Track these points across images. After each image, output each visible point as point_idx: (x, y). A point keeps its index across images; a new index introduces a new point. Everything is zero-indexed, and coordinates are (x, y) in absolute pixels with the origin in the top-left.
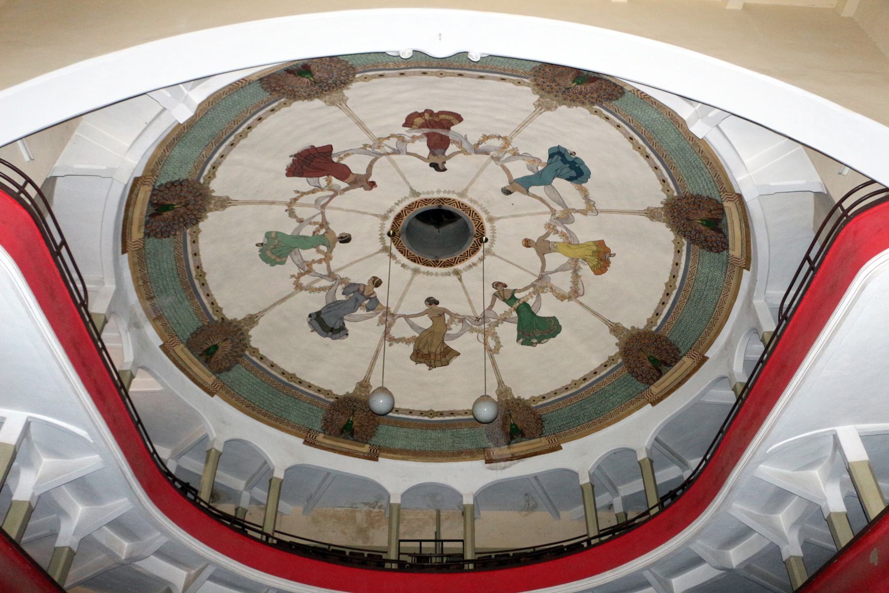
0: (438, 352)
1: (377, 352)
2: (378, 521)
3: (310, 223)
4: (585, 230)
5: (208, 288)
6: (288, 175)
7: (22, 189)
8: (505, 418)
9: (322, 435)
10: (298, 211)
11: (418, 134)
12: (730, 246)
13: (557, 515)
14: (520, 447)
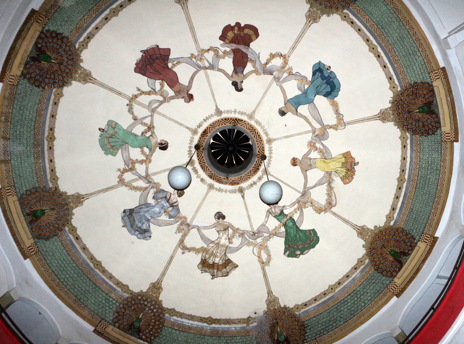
4: (336, 144)
5: (53, 153)
6: (136, 71)
8: (273, 327)
11: (228, 49)
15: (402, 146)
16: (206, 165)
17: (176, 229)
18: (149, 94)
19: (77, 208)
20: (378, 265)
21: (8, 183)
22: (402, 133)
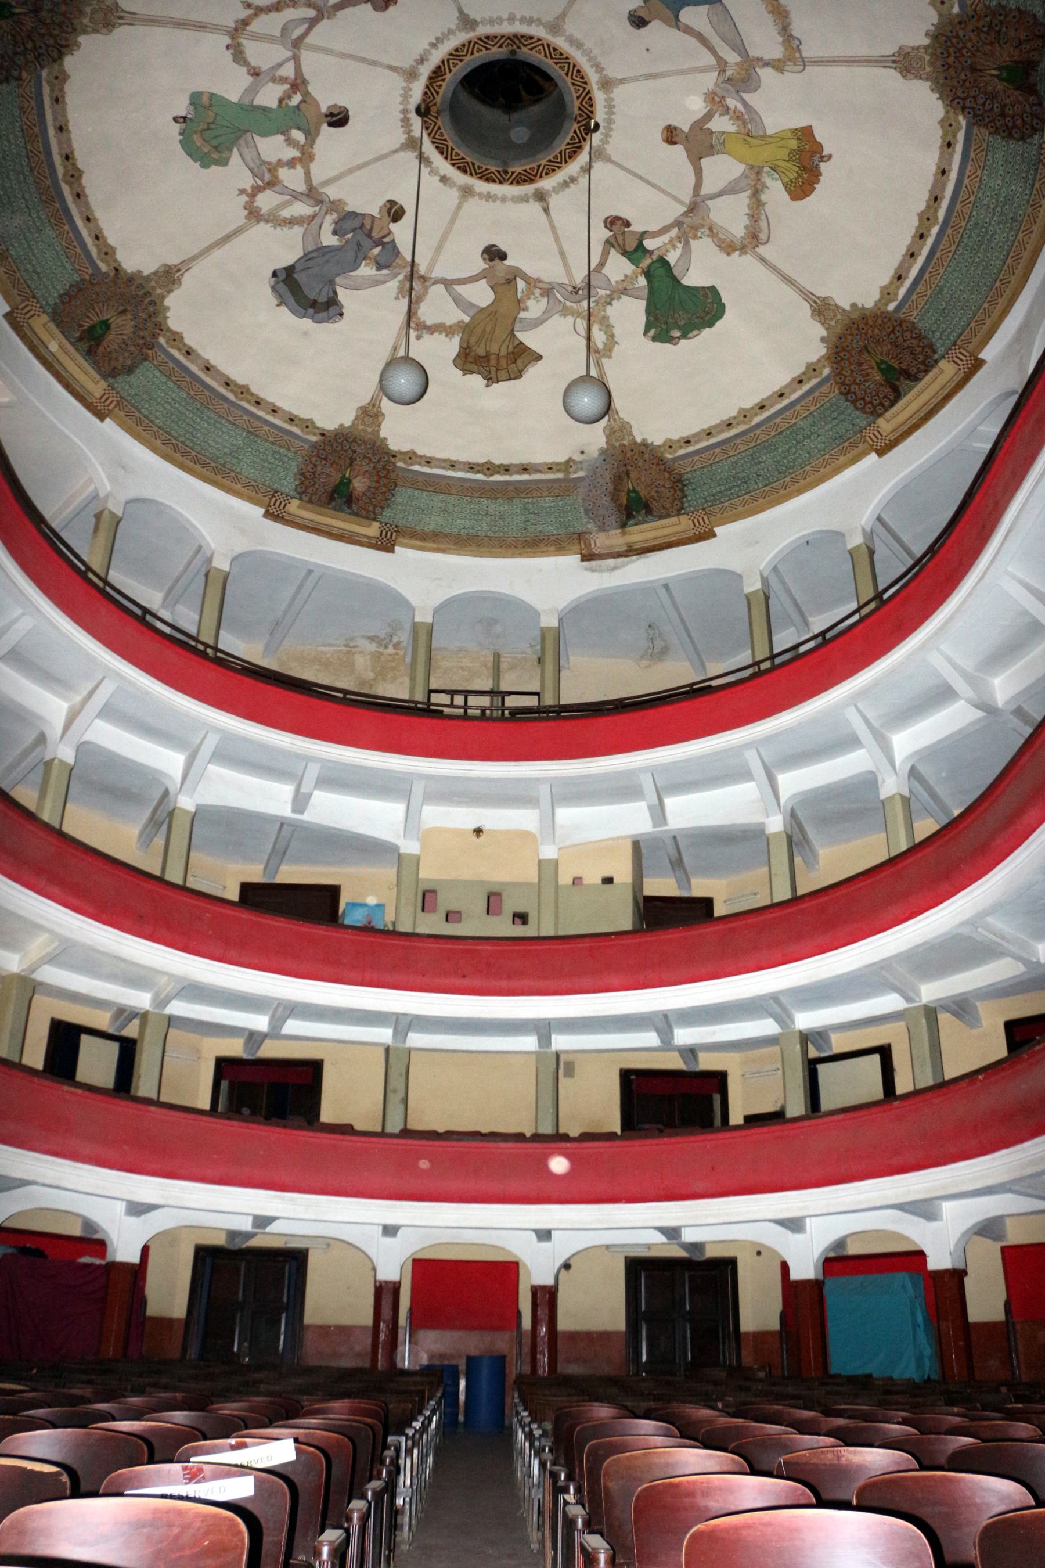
0: (503, 353)
2: (393, 669)
3: (273, 80)
5: (87, 204)
8: (618, 479)
9: (295, 503)
10: (252, 50)
14: (641, 533)
15: (944, 141)
16: (450, 144)
17: (395, 291)
18: (277, 10)
19: (172, 295)
20: (849, 385)
21: (20, 295)
22: (947, 112)
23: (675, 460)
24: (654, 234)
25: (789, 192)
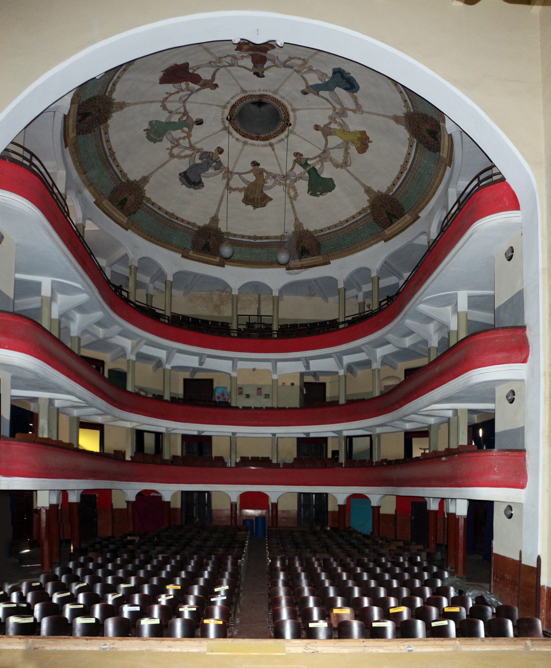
0: (259, 197)
1: (222, 197)
3: (177, 113)
4: (354, 123)
6: (160, 83)
7: (30, 161)
8: (298, 242)
9: (192, 251)
10: (168, 105)
12: (441, 150)
13: (326, 300)
14: (306, 261)
23: (317, 236)
24: (311, 159)
25: (358, 151)
